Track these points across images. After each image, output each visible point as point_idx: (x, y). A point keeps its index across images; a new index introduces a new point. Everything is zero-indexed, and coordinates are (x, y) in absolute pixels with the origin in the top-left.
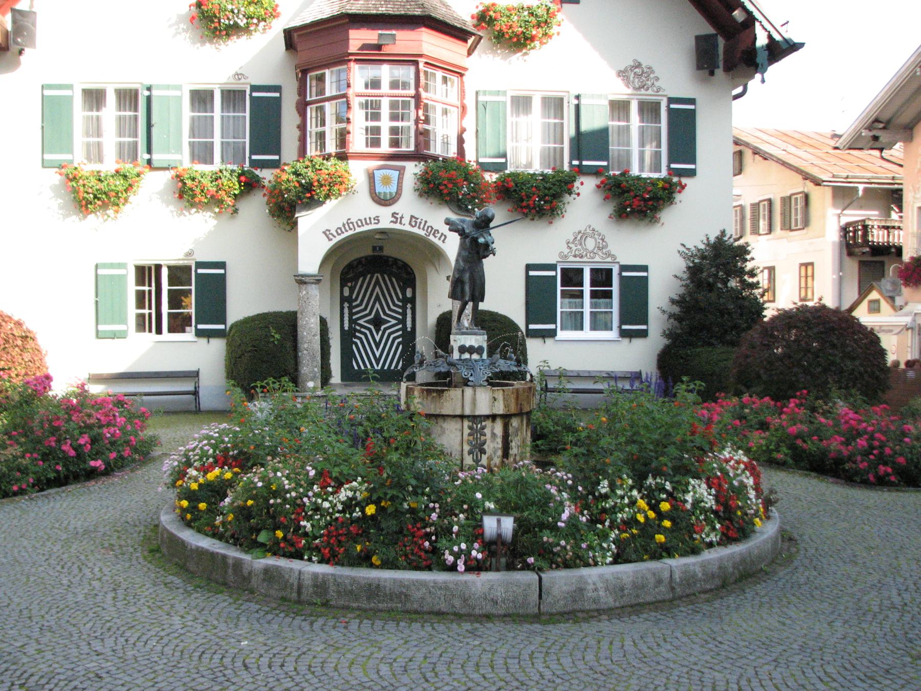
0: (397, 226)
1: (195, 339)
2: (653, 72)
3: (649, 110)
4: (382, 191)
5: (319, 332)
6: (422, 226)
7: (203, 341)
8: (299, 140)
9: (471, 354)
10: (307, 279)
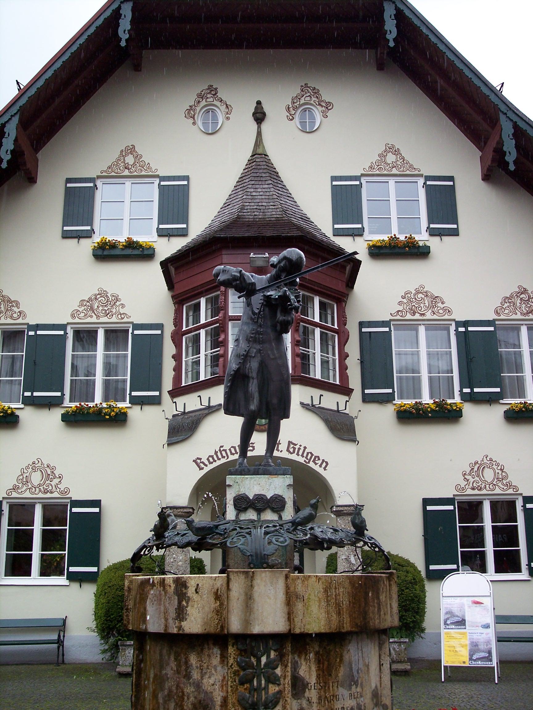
1: (67, 582)
2: (117, 300)
6: (300, 453)
7: (75, 586)
8: (174, 370)
9: (259, 511)
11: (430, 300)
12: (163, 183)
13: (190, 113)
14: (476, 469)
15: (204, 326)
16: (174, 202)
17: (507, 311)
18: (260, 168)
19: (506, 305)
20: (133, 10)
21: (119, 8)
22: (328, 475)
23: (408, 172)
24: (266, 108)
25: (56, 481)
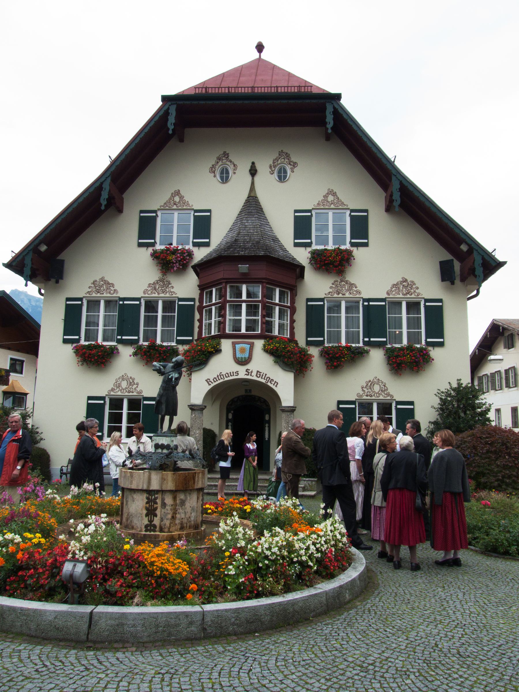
0: (249, 377)
2: (414, 284)
3: (413, 306)
4: (240, 357)
5: (202, 439)
9: (162, 449)
10: (195, 408)
11: (348, 285)
12: (196, 214)
13: (212, 170)
14: (369, 385)
15: (214, 304)
16: (202, 225)
17: (394, 293)
18: (252, 206)
19: (394, 289)
20: (177, 110)
21: (168, 109)
22: (278, 390)
23: (340, 207)
24: (258, 167)
25: (135, 386)
